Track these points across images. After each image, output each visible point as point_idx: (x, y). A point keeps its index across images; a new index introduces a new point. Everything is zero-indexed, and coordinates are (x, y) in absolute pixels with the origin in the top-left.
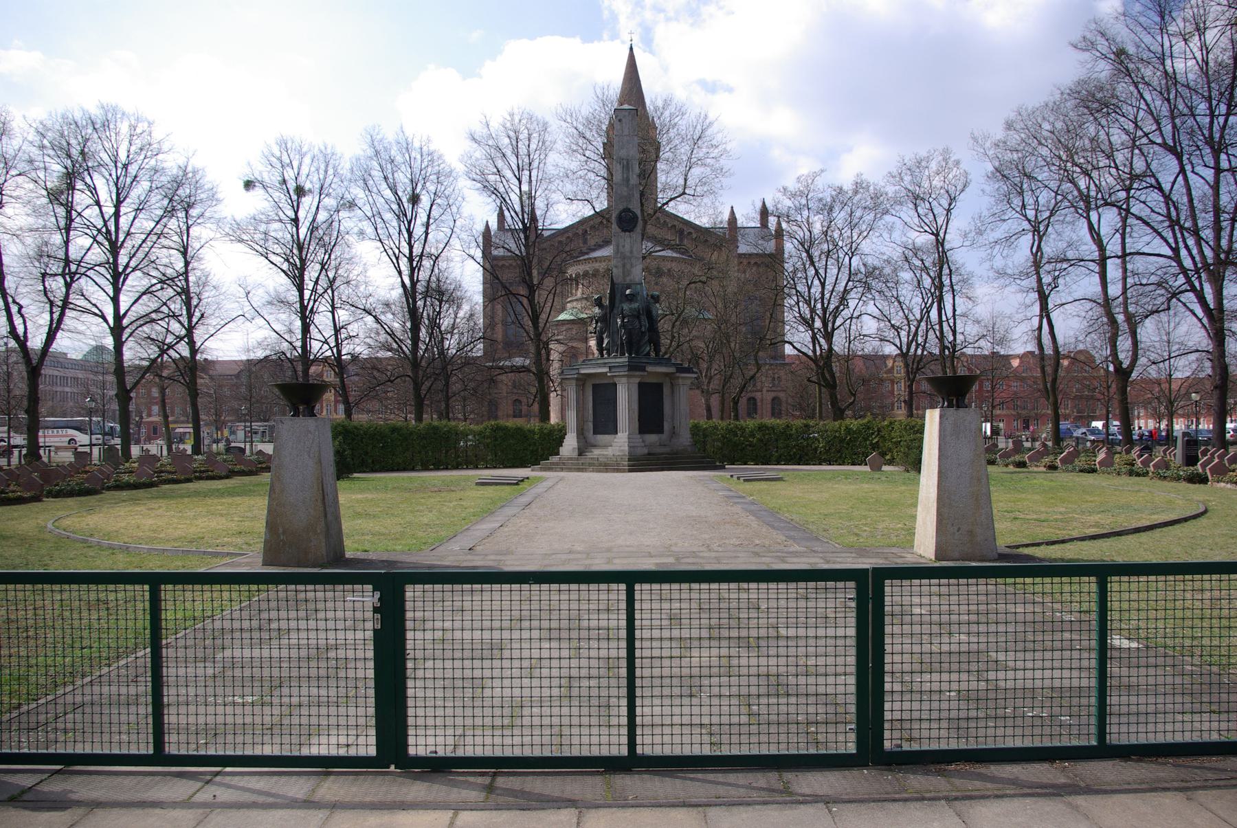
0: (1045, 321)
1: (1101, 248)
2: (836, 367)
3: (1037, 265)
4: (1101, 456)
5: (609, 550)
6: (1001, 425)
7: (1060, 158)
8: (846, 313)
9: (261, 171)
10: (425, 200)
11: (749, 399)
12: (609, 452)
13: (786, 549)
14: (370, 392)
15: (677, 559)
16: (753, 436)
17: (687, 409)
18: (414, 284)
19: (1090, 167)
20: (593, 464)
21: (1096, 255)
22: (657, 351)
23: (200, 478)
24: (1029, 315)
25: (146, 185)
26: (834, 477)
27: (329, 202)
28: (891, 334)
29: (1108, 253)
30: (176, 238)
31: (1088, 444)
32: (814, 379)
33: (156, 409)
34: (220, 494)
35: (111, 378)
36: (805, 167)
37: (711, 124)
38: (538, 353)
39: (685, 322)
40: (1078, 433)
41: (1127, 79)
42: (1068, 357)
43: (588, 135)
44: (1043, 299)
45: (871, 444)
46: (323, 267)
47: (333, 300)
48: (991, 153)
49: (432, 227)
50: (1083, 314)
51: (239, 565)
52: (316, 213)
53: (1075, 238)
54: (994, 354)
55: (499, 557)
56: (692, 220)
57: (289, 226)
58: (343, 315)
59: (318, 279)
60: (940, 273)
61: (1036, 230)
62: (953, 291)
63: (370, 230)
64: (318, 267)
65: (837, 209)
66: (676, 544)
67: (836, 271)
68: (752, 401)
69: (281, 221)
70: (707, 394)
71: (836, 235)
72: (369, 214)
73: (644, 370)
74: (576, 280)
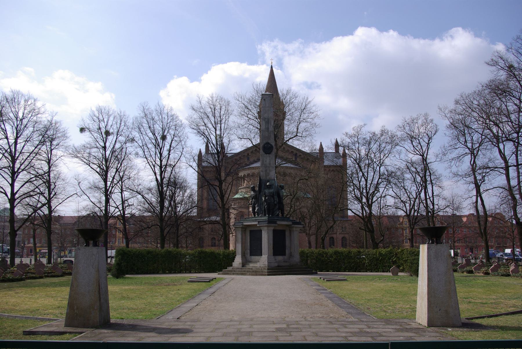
0: (479, 198)
1: (506, 162)
2: (374, 222)
3: (474, 170)
4: (512, 268)
5: (252, 320)
6: (459, 251)
7: (482, 117)
8: (378, 195)
9: (89, 123)
10: (169, 138)
11: (330, 238)
12: (258, 265)
13: (347, 320)
14: (137, 234)
15: (288, 325)
16: (332, 257)
17: (298, 243)
18: (162, 179)
19: (498, 122)
20: (250, 272)
21: (503, 165)
22: (283, 214)
23: (48, 276)
24: (471, 195)
25: (31, 129)
26: (373, 279)
27: (122, 139)
28: (401, 205)
29: (509, 164)
30: (45, 155)
31: (504, 261)
32: (363, 228)
33: (32, 240)
34: (55, 285)
35: (8, 224)
36: (355, 124)
37: (310, 102)
38: (224, 214)
39: (298, 199)
40: (499, 255)
41: (515, 79)
42: (491, 216)
43: (249, 107)
44: (478, 187)
45: (392, 261)
46: (117, 170)
47: (122, 187)
48: (448, 115)
49: (172, 151)
50: (499, 195)
51: (52, 326)
52: (115, 144)
53: (492, 157)
54: (454, 215)
55: (192, 323)
56: (300, 148)
57: (101, 150)
58: (126, 194)
59: (114, 176)
60: (425, 174)
61: (472, 153)
62: (432, 183)
63: (141, 153)
64: (115, 170)
65: (372, 143)
66: (288, 317)
67: (373, 174)
68: (332, 239)
69: (97, 147)
70: (309, 235)
71: (372, 156)
72: (141, 145)
73: (275, 223)
74: (243, 178)
